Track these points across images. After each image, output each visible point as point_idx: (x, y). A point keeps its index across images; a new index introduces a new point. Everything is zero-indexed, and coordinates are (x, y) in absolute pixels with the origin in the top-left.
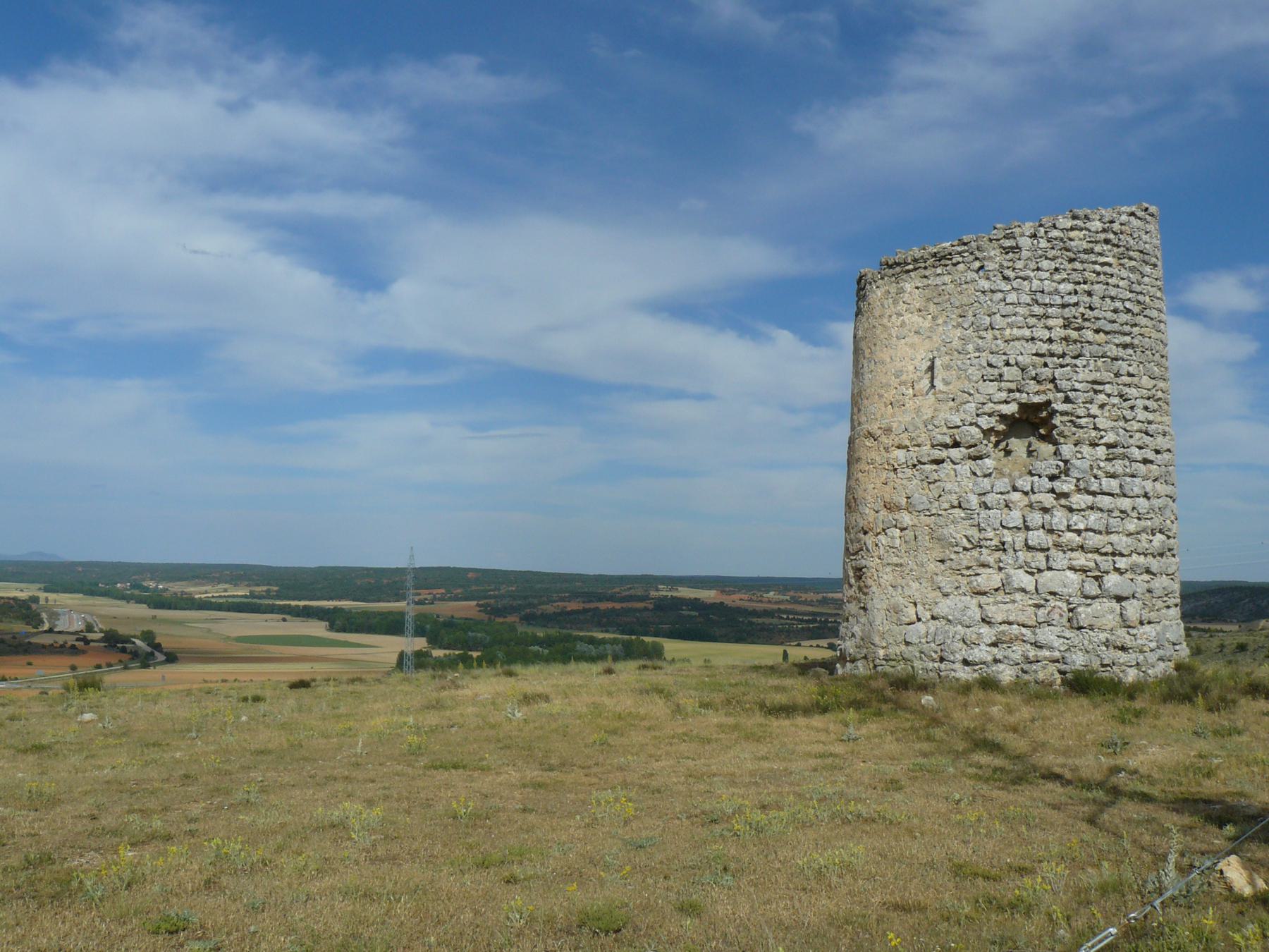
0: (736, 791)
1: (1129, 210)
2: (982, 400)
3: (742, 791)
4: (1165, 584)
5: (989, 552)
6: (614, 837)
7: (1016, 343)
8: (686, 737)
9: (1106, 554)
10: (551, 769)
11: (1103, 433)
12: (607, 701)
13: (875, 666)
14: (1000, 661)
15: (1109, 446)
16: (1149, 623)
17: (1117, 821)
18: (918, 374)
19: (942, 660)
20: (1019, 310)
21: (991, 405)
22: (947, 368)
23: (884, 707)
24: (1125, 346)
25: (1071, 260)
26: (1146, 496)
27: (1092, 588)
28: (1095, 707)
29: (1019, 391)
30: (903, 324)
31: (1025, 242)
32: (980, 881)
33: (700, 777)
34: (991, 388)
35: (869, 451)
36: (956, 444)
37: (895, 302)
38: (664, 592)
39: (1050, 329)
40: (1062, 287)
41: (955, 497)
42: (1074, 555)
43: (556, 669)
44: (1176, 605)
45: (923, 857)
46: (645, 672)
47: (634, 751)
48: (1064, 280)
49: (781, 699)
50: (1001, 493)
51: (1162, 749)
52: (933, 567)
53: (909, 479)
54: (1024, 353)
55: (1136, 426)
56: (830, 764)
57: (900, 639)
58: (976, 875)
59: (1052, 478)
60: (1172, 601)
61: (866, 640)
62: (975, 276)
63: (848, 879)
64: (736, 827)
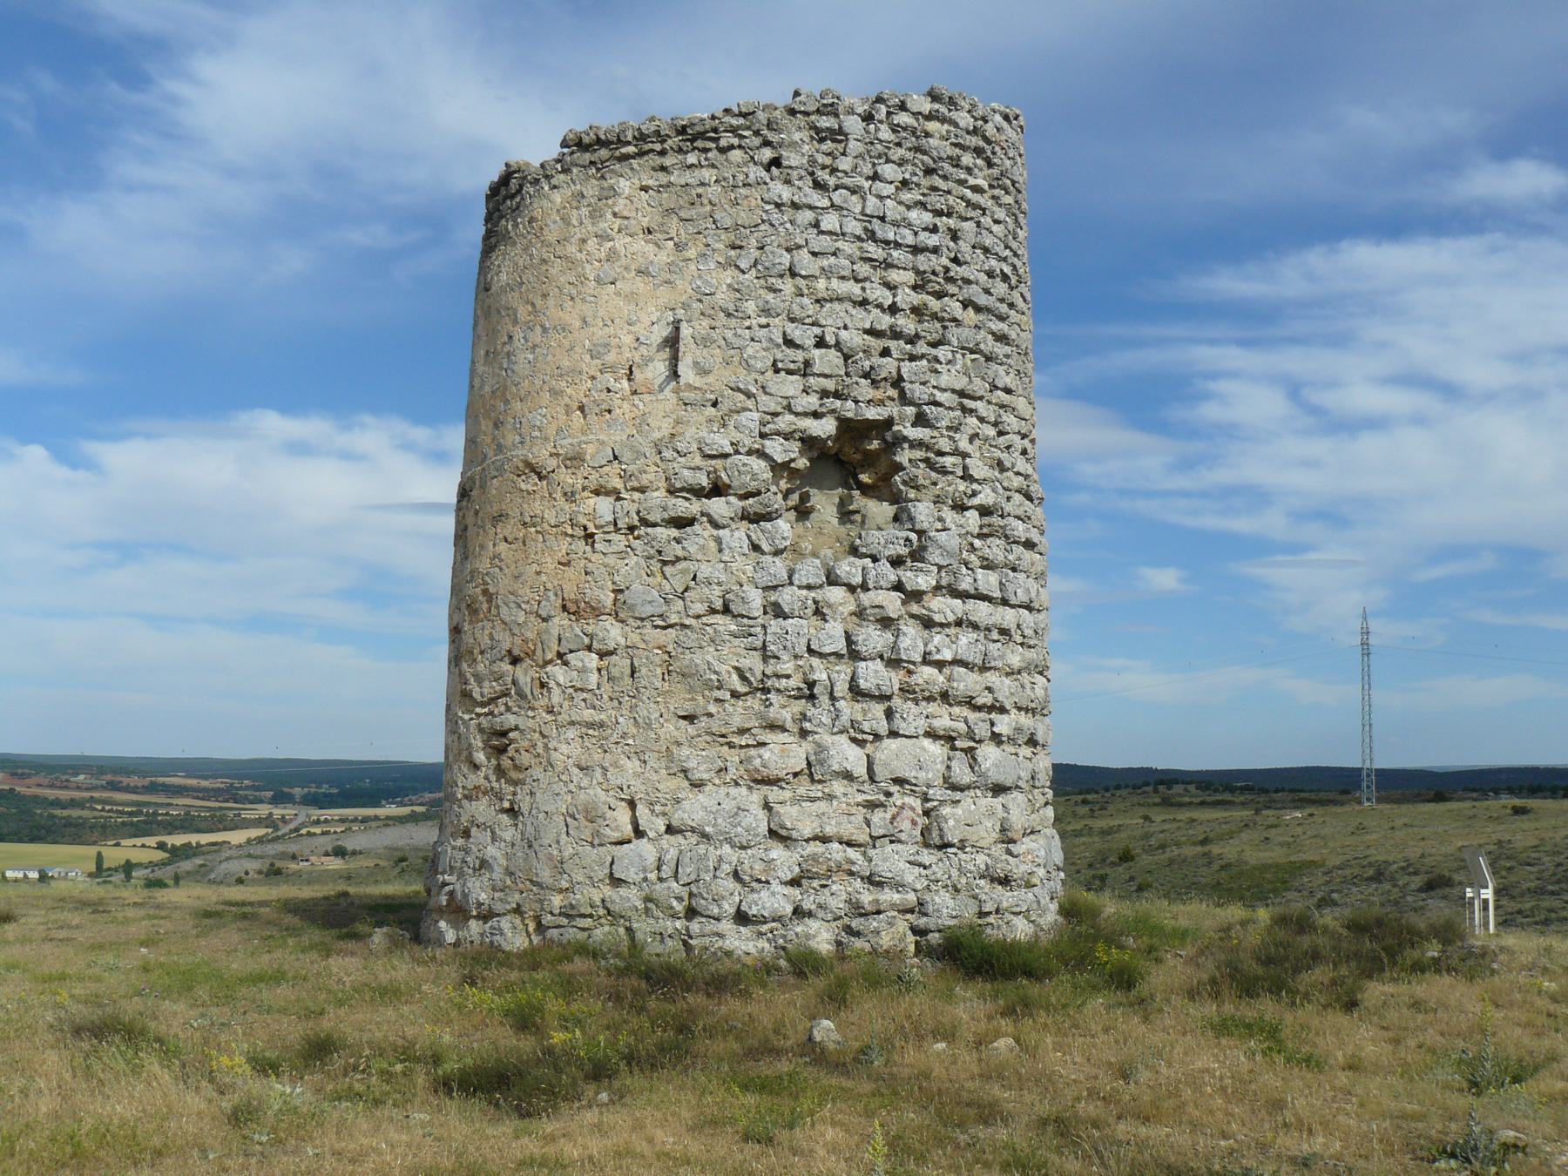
2: (773, 407)
5: (783, 700)
7: (836, 306)
11: (975, 486)
14: (810, 914)
15: (985, 511)
18: (643, 350)
19: (691, 913)
21: (790, 417)
22: (704, 342)
25: (929, 172)
27: (961, 773)
29: (837, 395)
30: (612, 256)
34: (790, 386)
36: (718, 490)
37: (596, 214)
40: (914, 215)
41: (717, 591)
42: (932, 708)
50: (809, 587)
52: (672, 729)
54: (850, 325)
55: (1017, 482)
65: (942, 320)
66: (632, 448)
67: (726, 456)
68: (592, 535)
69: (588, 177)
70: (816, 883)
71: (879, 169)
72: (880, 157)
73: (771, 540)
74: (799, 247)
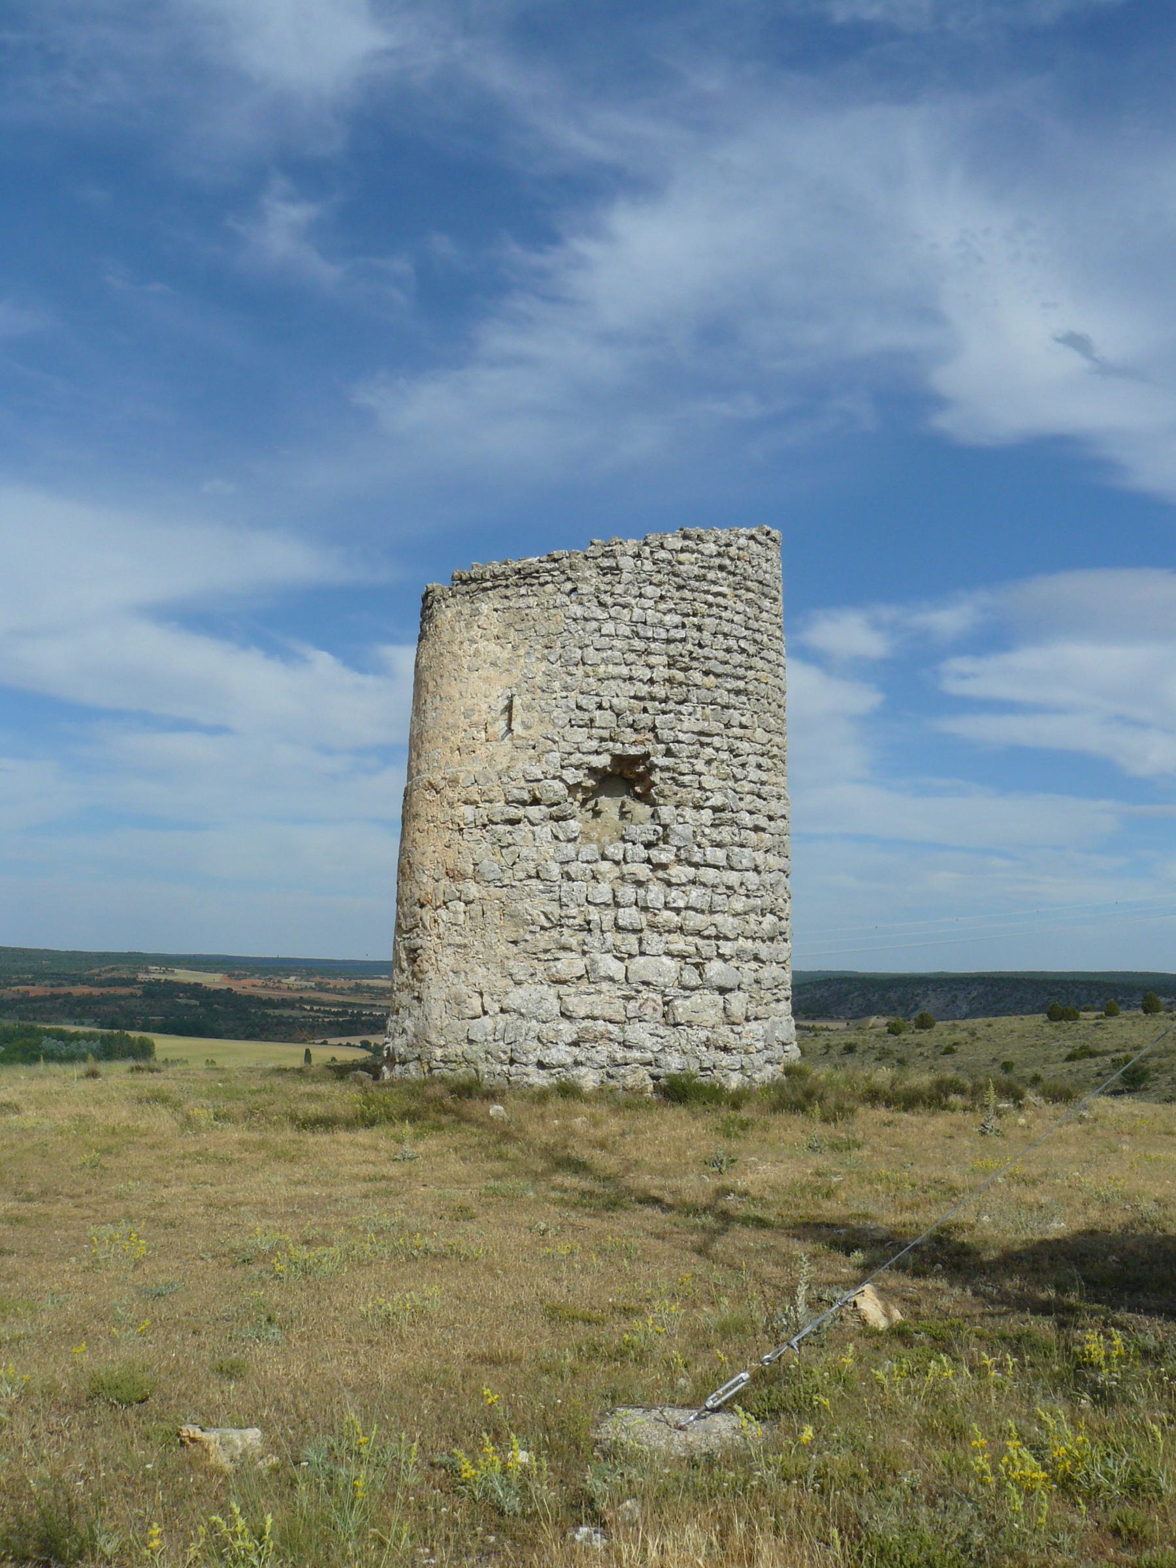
0: (270, 1223)
1: (748, 532)
2: (568, 749)
3: (278, 1224)
4: (775, 974)
5: (571, 932)
6: (123, 1283)
7: (612, 682)
8: (201, 1157)
9: (708, 937)
10: (30, 1198)
11: (709, 794)
12: (95, 1111)
13: (431, 1069)
14: (582, 1064)
15: (716, 810)
16: (756, 1019)
17: (732, 1250)
18: (493, 714)
19: (512, 1061)
20: (617, 643)
21: (579, 755)
22: (528, 708)
23: (444, 1119)
24: (738, 692)
25: (680, 588)
26: (756, 869)
27: (691, 977)
28: (694, 1119)
29: (612, 739)
31: (626, 563)
32: (580, 1325)
33: (223, 1207)
34: (580, 735)
35: (429, 807)
36: (536, 801)
37: (468, 626)
38: (156, 974)
39: (651, 667)
40: (667, 618)
41: (532, 864)
43: (22, 1072)
44: (787, 999)
45: (509, 1299)
46: (140, 1075)
47: (135, 1175)
48: (670, 611)
49: (315, 1109)
50: (588, 862)
51: (771, 1167)
52: (503, 949)
53: (478, 842)
54: (620, 695)
55: (748, 787)
56: (383, 1189)
57: (462, 1036)
58: (574, 1318)
59: (648, 845)
60: (782, 994)
61: (420, 1038)
62: (566, 599)
63: (423, 1327)
64: (278, 1267)
65: (688, 685)
66: (485, 775)
67: (539, 780)
68: (461, 830)
69: (465, 602)
70: (587, 1045)
71: (643, 591)
72: (644, 581)
73: (565, 832)
74: (587, 646)
